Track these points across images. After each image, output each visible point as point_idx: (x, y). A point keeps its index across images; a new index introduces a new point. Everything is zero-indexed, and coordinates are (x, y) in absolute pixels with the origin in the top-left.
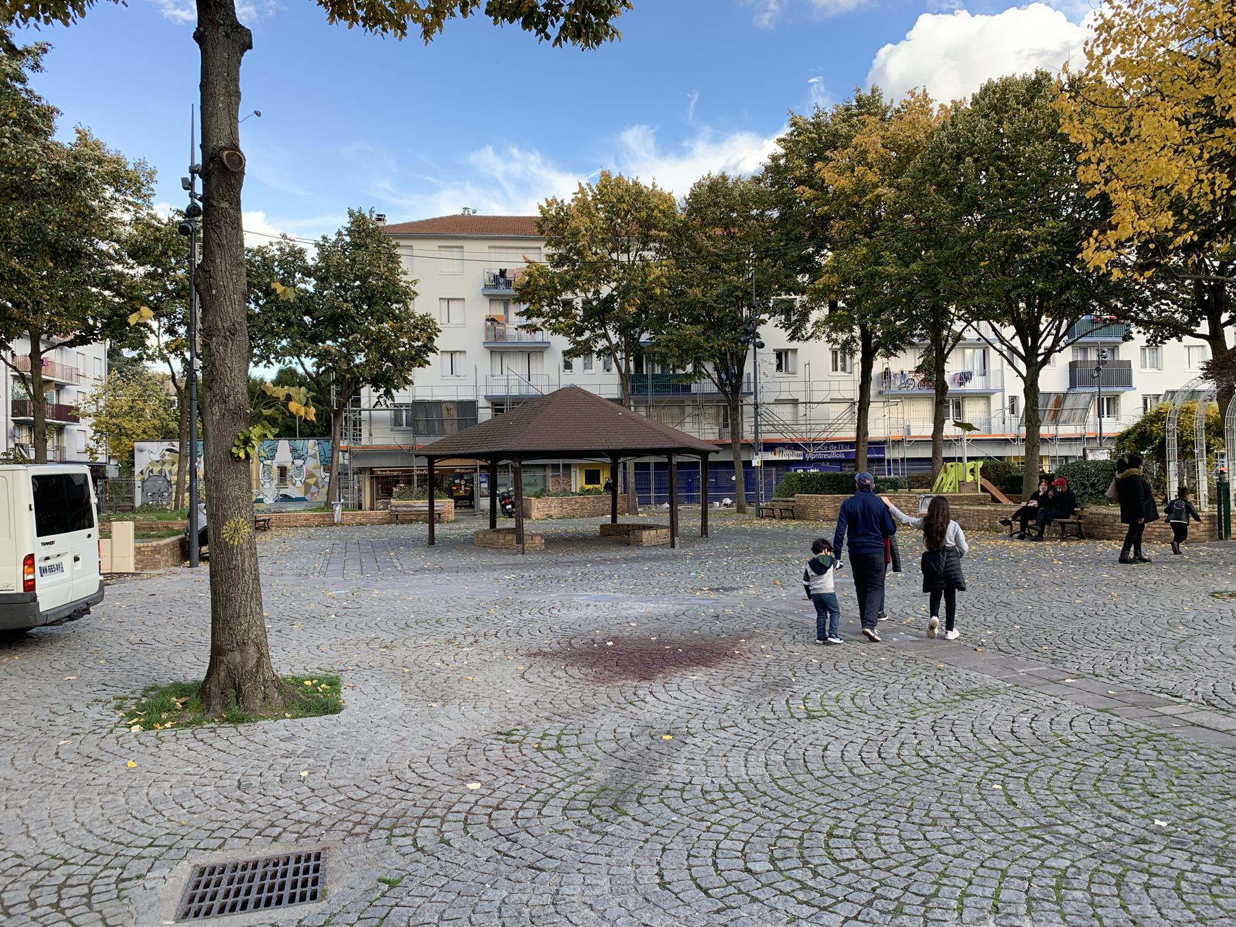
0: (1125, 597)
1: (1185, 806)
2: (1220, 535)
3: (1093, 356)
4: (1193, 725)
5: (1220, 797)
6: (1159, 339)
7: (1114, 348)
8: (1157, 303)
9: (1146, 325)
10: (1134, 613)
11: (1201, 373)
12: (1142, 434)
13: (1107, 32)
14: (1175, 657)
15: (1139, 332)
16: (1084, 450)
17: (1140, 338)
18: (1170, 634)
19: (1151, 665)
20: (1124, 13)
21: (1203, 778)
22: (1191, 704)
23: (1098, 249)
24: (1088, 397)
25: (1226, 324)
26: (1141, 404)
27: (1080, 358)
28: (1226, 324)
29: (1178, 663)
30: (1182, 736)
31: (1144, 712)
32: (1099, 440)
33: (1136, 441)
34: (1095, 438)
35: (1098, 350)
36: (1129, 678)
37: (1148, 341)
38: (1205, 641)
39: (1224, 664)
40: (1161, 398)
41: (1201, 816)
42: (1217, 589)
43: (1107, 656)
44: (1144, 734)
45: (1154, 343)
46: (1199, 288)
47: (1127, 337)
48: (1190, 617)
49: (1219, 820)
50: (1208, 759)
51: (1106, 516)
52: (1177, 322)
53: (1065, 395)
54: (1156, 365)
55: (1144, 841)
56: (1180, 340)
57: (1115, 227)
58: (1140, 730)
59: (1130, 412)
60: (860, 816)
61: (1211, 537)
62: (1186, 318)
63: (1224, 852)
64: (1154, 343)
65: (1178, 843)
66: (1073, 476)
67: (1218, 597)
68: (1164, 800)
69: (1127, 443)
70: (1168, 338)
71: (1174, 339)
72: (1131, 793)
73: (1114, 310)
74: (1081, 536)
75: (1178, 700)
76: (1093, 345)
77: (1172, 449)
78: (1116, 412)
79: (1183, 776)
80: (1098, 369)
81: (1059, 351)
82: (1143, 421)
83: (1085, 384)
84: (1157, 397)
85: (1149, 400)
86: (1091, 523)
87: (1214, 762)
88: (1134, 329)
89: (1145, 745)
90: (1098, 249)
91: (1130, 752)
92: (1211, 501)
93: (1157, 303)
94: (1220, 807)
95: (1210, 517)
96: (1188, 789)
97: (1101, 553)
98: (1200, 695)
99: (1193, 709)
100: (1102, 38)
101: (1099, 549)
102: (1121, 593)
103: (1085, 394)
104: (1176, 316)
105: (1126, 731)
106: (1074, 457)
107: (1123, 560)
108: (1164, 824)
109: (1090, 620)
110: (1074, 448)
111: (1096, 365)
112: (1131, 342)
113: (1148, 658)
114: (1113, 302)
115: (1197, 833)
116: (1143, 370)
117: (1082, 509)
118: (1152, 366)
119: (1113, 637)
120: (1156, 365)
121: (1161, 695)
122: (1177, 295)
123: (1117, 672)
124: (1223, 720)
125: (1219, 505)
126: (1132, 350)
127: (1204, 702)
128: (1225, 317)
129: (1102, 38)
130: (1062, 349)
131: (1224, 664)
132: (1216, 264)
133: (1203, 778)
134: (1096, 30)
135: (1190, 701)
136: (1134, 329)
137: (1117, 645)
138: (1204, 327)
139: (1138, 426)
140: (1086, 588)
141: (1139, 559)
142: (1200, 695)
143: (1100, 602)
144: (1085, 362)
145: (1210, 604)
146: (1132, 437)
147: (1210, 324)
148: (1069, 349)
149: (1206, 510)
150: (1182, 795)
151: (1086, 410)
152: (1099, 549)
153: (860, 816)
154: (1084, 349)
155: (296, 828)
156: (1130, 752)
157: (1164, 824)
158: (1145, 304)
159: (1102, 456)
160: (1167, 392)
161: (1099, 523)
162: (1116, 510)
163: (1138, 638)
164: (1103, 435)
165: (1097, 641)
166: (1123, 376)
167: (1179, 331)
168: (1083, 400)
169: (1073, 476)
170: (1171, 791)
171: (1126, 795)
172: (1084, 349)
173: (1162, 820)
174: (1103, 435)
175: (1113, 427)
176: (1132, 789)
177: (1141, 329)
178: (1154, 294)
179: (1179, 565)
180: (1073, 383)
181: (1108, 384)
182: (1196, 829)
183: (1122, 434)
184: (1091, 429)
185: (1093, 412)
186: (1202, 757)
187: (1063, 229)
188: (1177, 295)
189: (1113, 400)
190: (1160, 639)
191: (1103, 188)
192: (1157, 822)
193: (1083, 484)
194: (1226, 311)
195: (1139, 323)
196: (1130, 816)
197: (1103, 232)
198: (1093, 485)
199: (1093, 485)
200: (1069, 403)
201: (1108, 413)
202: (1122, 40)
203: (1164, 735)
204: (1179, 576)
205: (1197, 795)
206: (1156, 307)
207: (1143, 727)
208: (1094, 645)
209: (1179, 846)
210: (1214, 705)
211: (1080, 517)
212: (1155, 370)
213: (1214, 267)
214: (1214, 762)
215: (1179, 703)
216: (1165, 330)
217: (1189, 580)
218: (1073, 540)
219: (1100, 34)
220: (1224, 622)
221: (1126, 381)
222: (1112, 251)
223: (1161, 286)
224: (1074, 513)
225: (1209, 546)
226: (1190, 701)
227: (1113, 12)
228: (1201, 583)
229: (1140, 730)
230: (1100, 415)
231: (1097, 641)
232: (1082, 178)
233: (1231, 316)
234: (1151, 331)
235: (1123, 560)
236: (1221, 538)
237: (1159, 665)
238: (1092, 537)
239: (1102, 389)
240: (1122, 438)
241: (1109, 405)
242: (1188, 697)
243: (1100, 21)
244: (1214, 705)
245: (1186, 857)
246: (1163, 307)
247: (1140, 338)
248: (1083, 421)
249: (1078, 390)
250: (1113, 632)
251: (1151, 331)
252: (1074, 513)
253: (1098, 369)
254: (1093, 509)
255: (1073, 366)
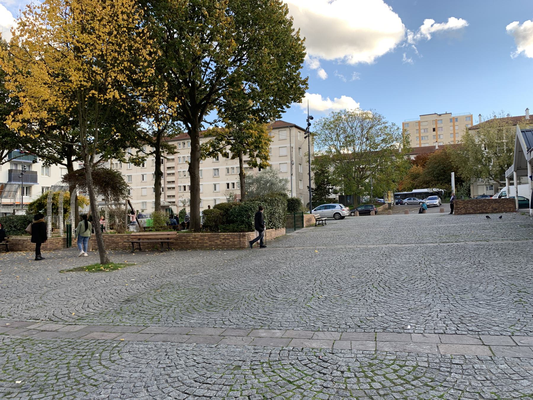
0: (23, 277)
1: (31, 370)
2: (67, 246)
3: (20, 168)
4: (42, 331)
5: (47, 361)
6: (48, 164)
7: (30, 166)
8: (48, 149)
9: (43, 157)
10: (26, 284)
11: (61, 180)
12: (40, 204)
13: (23, 26)
14: (40, 302)
15: (40, 160)
16: (14, 210)
17: (40, 162)
18: (39, 292)
19: (29, 307)
20: (31, 22)
21: (41, 354)
22: (43, 322)
23: (13, 121)
24: (17, 186)
25: (74, 160)
26: (41, 191)
27: (14, 168)
28: (74, 160)
29: (41, 304)
30: (35, 338)
31: (22, 330)
32: (21, 205)
33: (37, 206)
34: (20, 205)
35: (22, 166)
36: (17, 315)
37: (43, 164)
38: (53, 292)
39: (59, 301)
40: (49, 188)
41: (37, 373)
42: (62, 269)
43: (9, 307)
44: (19, 341)
45: (46, 165)
46: (63, 146)
47: (35, 162)
48: (49, 283)
49: (45, 372)
50: (45, 345)
51: (20, 240)
52: (55, 157)
53: (6, 184)
54: (48, 174)
55: (9, 393)
56: (57, 165)
57: (21, 112)
58: (18, 339)
59: (36, 193)
60: (111, 350)
61: (64, 247)
62: (59, 156)
63: (44, 387)
64: (46, 165)
65: (25, 389)
66: (5, 222)
67: (62, 273)
68: (22, 370)
69: (33, 207)
70: (52, 164)
71: (54, 164)
72: (7, 372)
73: (28, 148)
74: (7, 250)
75: (37, 321)
76: (20, 163)
77: (50, 210)
78: (30, 193)
79: (33, 356)
80: (22, 174)
81: (2, 164)
82: (41, 198)
83: (15, 180)
84: (48, 188)
85: (44, 189)
86: (12, 244)
87: (47, 346)
88: (38, 159)
89: (18, 346)
90: (13, 121)
91: (11, 351)
92: (65, 232)
93: (48, 149)
94: (46, 366)
95: (64, 239)
96: (34, 362)
97: (16, 258)
98: (47, 317)
99: (43, 324)
100: (20, 28)
101: (15, 256)
102: (21, 276)
103: (16, 184)
104: (55, 155)
105: (11, 341)
106: (10, 213)
107: (36, 259)
108: (20, 382)
109: (4, 290)
110: (10, 210)
111: (21, 172)
112: (36, 164)
113: (28, 304)
114: (29, 145)
115: (34, 381)
116: (42, 176)
117: (8, 238)
118: (46, 175)
119: (13, 297)
120: (48, 174)
121: (30, 321)
122: (56, 146)
123: (12, 313)
124: (55, 326)
125: (67, 234)
126: (38, 167)
127: (49, 320)
128: (73, 158)
129: (20, 28)
130: (4, 163)
131: (59, 301)
132: (71, 136)
133: (41, 354)
134: (18, 24)
135: (42, 320)
136: (38, 159)
137: (15, 300)
138: (65, 161)
139: (38, 200)
140: (5, 275)
141: (42, 259)
142: (47, 317)
143: (10, 281)
144: (16, 170)
145: (58, 276)
146: (35, 205)
147: (68, 160)
148: (8, 164)
149: (62, 236)
150: (31, 365)
151: (16, 192)
152: (15, 256)
153: (111, 350)
154: (16, 164)
155: (247, 321)
156: (11, 351)
157: (20, 382)
158: (43, 148)
159: (22, 213)
160: (52, 186)
161: (16, 244)
162: (29, 237)
163: (25, 296)
164: (23, 203)
165: (5, 300)
166: (33, 178)
167: (57, 161)
168: (14, 188)
169: (5, 222)
170: (26, 365)
171: (5, 373)
172: (16, 164)
173: (19, 380)
174: (23, 203)
175: (28, 200)
176: (8, 369)
177: (41, 158)
178: (46, 145)
179: (49, 260)
180: (10, 180)
181: (27, 181)
182: (34, 380)
183: (31, 203)
184: (18, 201)
185: (19, 193)
186: (43, 345)
187: (5, 108)
188: (56, 146)
189: (29, 188)
190: (35, 295)
191: (17, 94)
192: (17, 382)
193: (10, 226)
194: (74, 156)
195: (40, 156)
196: (5, 383)
197: (15, 114)
198: (15, 227)
199: (15, 227)
200: (7, 188)
201: (26, 194)
202: (29, 33)
203: (28, 339)
204: (48, 265)
205: (37, 363)
206: (47, 150)
207: (19, 337)
208: (3, 303)
209: (25, 391)
210: (52, 320)
211: (7, 242)
212: (47, 177)
213: (70, 137)
214: (47, 346)
215: (38, 323)
216: (50, 160)
217: (52, 266)
218: (3, 252)
219: (20, 27)
220: (62, 283)
221: (34, 180)
222: (20, 123)
223: (49, 142)
224: (4, 240)
225: (63, 251)
226: (42, 320)
227: (26, 19)
228: (56, 267)
229: (18, 339)
230: (23, 194)
231: (5, 300)
232: (7, 87)
233: (76, 158)
234: (45, 160)
235: (36, 259)
236: (68, 247)
237: (32, 306)
238: (13, 250)
239: (24, 183)
240: (31, 205)
241: (27, 190)
242: (42, 319)
243: (20, 21)
244: (52, 320)
245: (27, 395)
246: (50, 151)
247: (40, 162)
248: (14, 197)
249: (12, 183)
250: (14, 295)
251: (45, 160)
252: (4, 240)
253: (22, 174)
254: (14, 237)
255: (10, 171)
